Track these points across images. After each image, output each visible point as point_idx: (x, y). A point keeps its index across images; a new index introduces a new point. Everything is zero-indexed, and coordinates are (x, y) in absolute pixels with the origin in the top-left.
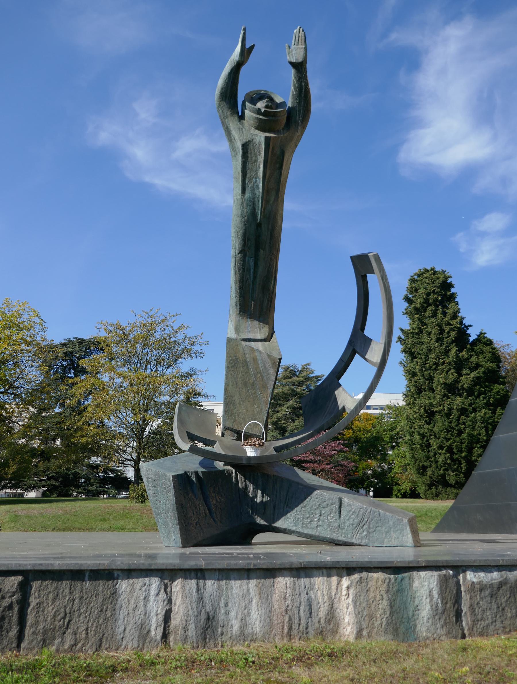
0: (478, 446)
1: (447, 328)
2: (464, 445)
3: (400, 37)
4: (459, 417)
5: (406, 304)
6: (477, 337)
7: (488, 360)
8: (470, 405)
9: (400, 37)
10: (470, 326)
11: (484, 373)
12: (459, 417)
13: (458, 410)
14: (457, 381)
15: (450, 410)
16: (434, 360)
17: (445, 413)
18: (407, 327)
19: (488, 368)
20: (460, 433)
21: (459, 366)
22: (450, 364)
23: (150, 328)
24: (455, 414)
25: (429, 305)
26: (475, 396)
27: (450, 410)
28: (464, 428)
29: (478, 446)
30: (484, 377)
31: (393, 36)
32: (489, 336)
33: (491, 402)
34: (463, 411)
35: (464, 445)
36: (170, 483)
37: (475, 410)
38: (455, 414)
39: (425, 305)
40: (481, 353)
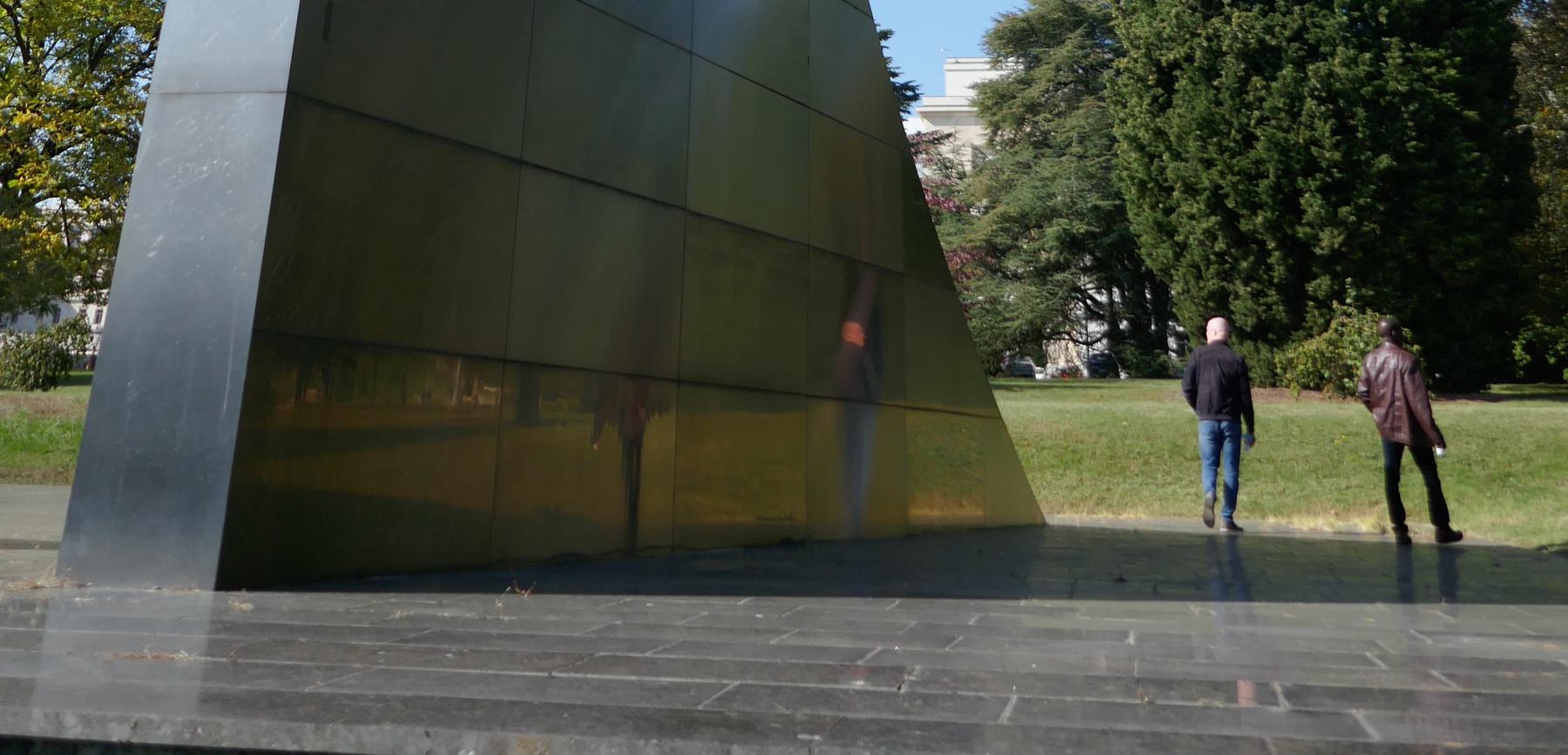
0: (1313, 184)
2: (1264, 184)
4: (1244, 81)
8: (1298, 36)
13: (1244, 55)
15: (1215, 54)
17: (1200, 68)
20: (1249, 140)
24: (1231, 68)
27: (1215, 54)
28: (1260, 122)
29: (1313, 184)
33: (1383, 20)
34: (1262, 60)
37: (1314, 54)
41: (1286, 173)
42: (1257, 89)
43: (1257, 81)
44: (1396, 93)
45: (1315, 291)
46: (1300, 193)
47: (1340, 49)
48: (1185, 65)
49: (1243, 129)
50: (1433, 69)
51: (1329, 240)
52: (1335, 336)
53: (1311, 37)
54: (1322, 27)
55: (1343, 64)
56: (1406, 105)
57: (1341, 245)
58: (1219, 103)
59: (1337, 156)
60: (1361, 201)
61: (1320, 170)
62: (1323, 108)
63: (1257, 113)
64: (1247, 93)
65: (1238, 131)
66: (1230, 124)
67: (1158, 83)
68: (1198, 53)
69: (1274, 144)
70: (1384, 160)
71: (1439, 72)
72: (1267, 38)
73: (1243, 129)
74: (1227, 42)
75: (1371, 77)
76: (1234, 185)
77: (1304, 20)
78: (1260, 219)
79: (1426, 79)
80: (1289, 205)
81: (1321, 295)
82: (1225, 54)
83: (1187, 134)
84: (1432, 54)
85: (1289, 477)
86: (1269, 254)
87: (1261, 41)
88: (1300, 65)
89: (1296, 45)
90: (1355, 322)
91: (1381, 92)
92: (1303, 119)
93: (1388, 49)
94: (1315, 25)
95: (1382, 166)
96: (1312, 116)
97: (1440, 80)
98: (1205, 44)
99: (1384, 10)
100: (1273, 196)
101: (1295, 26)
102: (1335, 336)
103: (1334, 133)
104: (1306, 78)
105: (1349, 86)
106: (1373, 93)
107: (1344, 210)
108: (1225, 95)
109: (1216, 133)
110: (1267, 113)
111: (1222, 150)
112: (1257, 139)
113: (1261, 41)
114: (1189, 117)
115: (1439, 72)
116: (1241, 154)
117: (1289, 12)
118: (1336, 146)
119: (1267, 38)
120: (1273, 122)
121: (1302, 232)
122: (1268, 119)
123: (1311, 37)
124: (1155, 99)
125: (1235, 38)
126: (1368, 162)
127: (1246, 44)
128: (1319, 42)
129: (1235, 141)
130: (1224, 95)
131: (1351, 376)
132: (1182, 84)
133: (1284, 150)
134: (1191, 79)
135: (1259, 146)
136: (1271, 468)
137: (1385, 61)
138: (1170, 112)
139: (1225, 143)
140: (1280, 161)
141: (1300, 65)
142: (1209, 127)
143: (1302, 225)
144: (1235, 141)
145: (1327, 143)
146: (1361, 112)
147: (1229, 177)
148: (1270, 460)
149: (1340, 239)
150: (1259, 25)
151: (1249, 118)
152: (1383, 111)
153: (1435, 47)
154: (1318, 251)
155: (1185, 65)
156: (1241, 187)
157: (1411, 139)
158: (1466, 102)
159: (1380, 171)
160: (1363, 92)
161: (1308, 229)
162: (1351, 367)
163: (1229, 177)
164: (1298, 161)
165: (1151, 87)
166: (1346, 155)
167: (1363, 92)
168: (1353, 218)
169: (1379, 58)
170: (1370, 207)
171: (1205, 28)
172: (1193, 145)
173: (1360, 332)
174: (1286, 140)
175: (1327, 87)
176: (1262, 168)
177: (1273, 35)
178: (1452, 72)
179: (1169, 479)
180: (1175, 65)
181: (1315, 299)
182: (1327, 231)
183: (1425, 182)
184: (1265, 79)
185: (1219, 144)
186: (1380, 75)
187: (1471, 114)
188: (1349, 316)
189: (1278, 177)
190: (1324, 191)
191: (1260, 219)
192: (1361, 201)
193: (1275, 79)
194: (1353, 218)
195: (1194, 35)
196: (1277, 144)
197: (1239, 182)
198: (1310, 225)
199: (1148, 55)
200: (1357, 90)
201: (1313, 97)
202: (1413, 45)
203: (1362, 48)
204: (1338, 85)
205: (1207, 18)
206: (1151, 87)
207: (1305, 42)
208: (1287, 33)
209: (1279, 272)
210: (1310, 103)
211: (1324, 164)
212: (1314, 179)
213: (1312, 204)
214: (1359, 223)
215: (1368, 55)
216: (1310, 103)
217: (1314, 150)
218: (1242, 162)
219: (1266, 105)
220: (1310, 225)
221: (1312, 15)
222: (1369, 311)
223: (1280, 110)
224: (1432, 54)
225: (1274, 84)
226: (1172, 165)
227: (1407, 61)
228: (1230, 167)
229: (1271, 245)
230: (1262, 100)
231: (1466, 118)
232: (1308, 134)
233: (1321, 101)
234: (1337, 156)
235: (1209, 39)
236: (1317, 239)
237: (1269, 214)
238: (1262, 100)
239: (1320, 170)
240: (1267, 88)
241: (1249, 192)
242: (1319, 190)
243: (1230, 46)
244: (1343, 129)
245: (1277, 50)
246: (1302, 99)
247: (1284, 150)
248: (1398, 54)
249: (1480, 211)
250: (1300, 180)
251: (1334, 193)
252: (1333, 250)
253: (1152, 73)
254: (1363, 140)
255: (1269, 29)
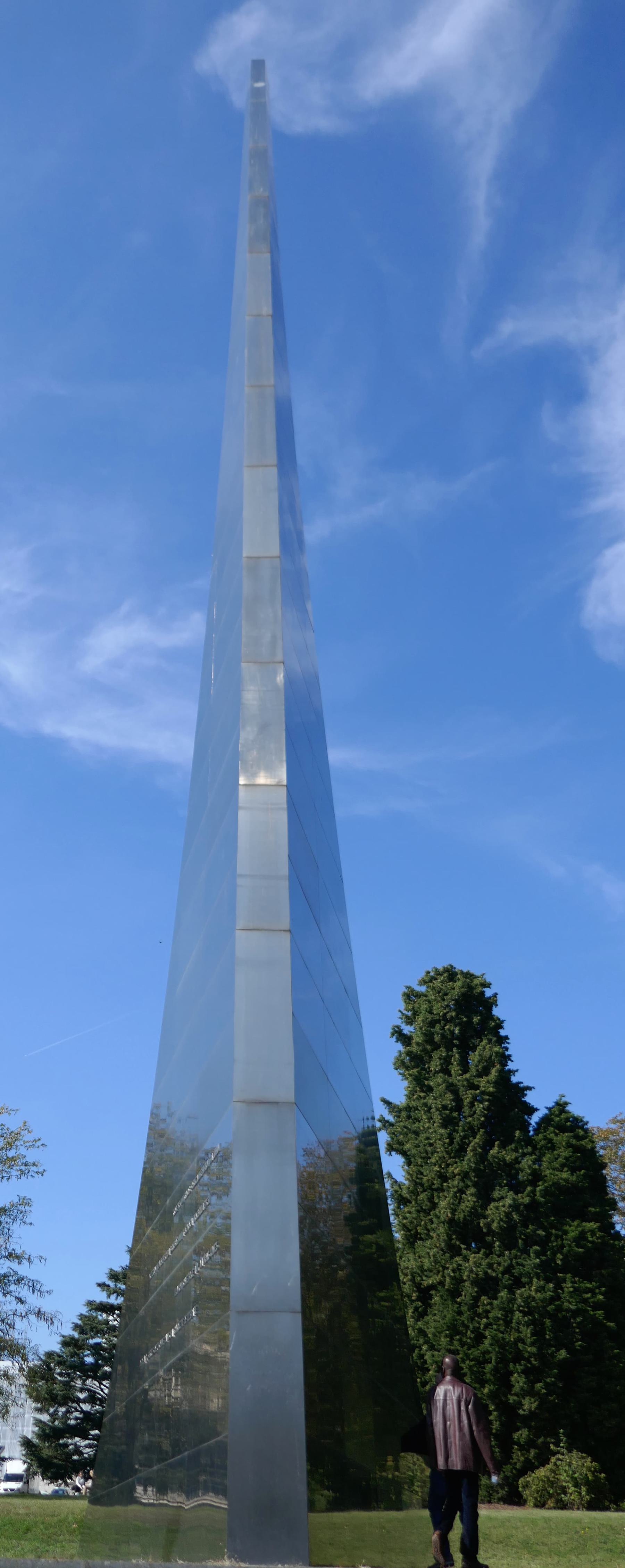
0: (519, 1368)
1: (467, 1097)
2: (489, 1367)
3: (523, 328)
4: (476, 1299)
5: (400, 1047)
6: (547, 1112)
7: (563, 1166)
8: (508, 1270)
9: (523, 328)
10: (530, 1088)
11: (546, 1193)
12: (476, 1299)
13: (475, 1282)
14: (476, 1213)
15: (458, 1281)
16: (436, 1168)
17: (448, 1290)
18: (400, 1098)
19: (556, 1184)
20: (479, 1338)
21: (486, 1180)
22: (465, 1175)
23: (410, 996)
24: (468, 1290)
25: (436, 1047)
26: (519, 1250)
27: (458, 1281)
28: (487, 1326)
29: (519, 1368)
30: (546, 1202)
31: (507, 328)
32: (575, 1109)
33: (559, 1262)
34: (487, 1285)
35: (489, 1367)
36: (249, 64)
37: (517, 1283)
38: (468, 1290)
39: (429, 1047)
40: (548, 1149)
41: (503, 1360)
42: (484, 1305)
43: (484, 1299)
44: (568, 1310)
45: (518, 1439)
46: (511, 1373)
47: (535, 1280)
48: (439, 1288)
49: (476, 1330)
50: (589, 1295)
51: (529, 1404)
52: (554, 1468)
53: (516, 1272)
54: (523, 1266)
55: (537, 1291)
56: (575, 1318)
57: (536, 1408)
58: (460, 1313)
59: (534, 1350)
60: (548, 1380)
61: (524, 1359)
62: (526, 1319)
63: (485, 1320)
64: (478, 1307)
65: (472, 1332)
66: (467, 1327)
67: (419, 1299)
68: (448, 1279)
69: (495, 1341)
70: (563, 1354)
71: (592, 1297)
72: (489, 1271)
73: (476, 1330)
74: (466, 1273)
75: (552, 1300)
76: (470, 1368)
77: (511, 1260)
78: (486, 1390)
79: (585, 1301)
80: (503, 1380)
81: (522, 1441)
82: (464, 1281)
83: (440, 1333)
84: (589, 1285)
85: (559, 1554)
86: (490, 1413)
87: (486, 1273)
88: (511, 1291)
89: (507, 1276)
90: (567, 1458)
91: (559, 1309)
92: (513, 1325)
93: (564, 1281)
94: (518, 1264)
95: (561, 1357)
96: (519, 1323)
97: (593, 1302)
98: (452, 1274)
99: (559, 1256)
100: (494, 1375)
101: (506, 1264)
102: (554, 1468)
103: (533, 1334)
104: (515, 1299)
105: (540, 1304)
106: (554, 1310)
107: (539, 1385)
108: (464, 1308)
109: (458, 1334)
110: (491, 1321)
111: (463, 1344)
112: (486, 1337)
113: (486, 1273)
114: (442, 1322)
115: (592, 1297)
116: (473, 1347)
117: (501, 1255)
118: (533, 1344)
119: (489, 1271)
120: (495, 1327)
121: (512, 1399)
122: (491, 1324)
123: (516, 1272)
124: (416, 1309)
125: (471, 1271)
126: (552, 1355)
127: (477, 1275)
128: (521, 1275)
129: (470, 1338)
130: (464, 1308)
131: (565, 1493)
132: (436, 1299)
133: (502, 1344)
134: (442, 1296)
135: (487, 1342)
136: (546, 1548)
137: (562, 1289)
138: (426, 1318)
139: (464, 1339)
140: (499, 1352)
141: (511, 1291)
142: (454, 1330)
143: (512, 1395)
144: (470, 1338)
145: (529, 1341)
146: (548, 1322)
147: (467, 1362)
148: (544, 1544)
149: (534, 1405)
150: (484, 1263)
151: (479, 1323)
152: (562, 1322)
153: (590, 1282)
154: (521, 1412)
155: (439, 1288)
156: (475, 1369)
157: (578, 1340)
158: (608, 1317)
159: (560, 1361)
160: (549, 1309)
161: (515, 1398)
162: (565, 1487)
163: (467, 1362)
164: (510, 1353)
165: (413, 1301)
166: (540, 1349)
167: (549, 1309)
168: (544, 1391)
169: (559, 1286)
170: (553, 1384)
171: (452, 1263)
172: (444, 1341)
173: (570, 1465)
174: (503, 1339)
175: (527, 1304)
176: (487, 1357)
177: (494, 1270)
178: (601, 1297)
179: (489, 1555)
180: (432, 1287)
181: (518, 1444)
182: (527, 1398)
183: (586, 1368)
184: (489, 1298)
185: (460, 1340)
186: (558, 1298)
187: (612, 1324)
188: (563, 1454)
189: (497, 1363)
190: (526, 1372)
191: (486, 1390)
192: (548, 1380)
193: (496, 1299)
194: (544, 1391)
195: (445, 1268)
196: (497, 1341)
197: (474, 1366)
198: (516, 1395)
199: (413, 1280)
200: (545, 1307)
201: (520, 1311)
202: (577, 1279)
203: (548, 1281)
204: (533, 1304)
205: (452, 1257)
206: (413, 1301)
207: (512, 1275)
208: (501, 1269)
209: (496, 1425)
210: (518, 1315)
211: (526, 1355)
212: (521, 1365)
213: (518, 1381)
214: (547, 1394)
215: (551, 1285)
216: (518, 1315)
217: (520, 1346)
218: (475, 1353)
219: (491, 1315)
220: (516, 1395)
221: (516, 1257)
222: (575, 1452)
223: (499, 1319)
224: (589, 1285)
225: (495, 1302)
226: (429, 1354)
227: (576, 1290)
228: (467, 1355)
229: (492, 1407)
230: (488, 1312)
231: (609, 1327)
232: (517, 1335)
233: (525, 1314)
234: (534, 1350)
235: (454, 1271)
236: (521, 1405)
237: (492, 1387)
238: (488, 1312)
239: (524, 1359)
240: (491, 1304)
241: (479, 1372)
242: (523, 1372)
243: (468, 1276)
244: (539, 1333)
245: (496, 1280)
246: (512, 1312)
247: (502, 1344)
248: (570, 1285)
249: (618, 1388)
250: (511, 1365)
251: (533, 1375)
252: (530, 1410)
253: (414, 1291)
254: (549, 1340)
255: (490, 1266)
